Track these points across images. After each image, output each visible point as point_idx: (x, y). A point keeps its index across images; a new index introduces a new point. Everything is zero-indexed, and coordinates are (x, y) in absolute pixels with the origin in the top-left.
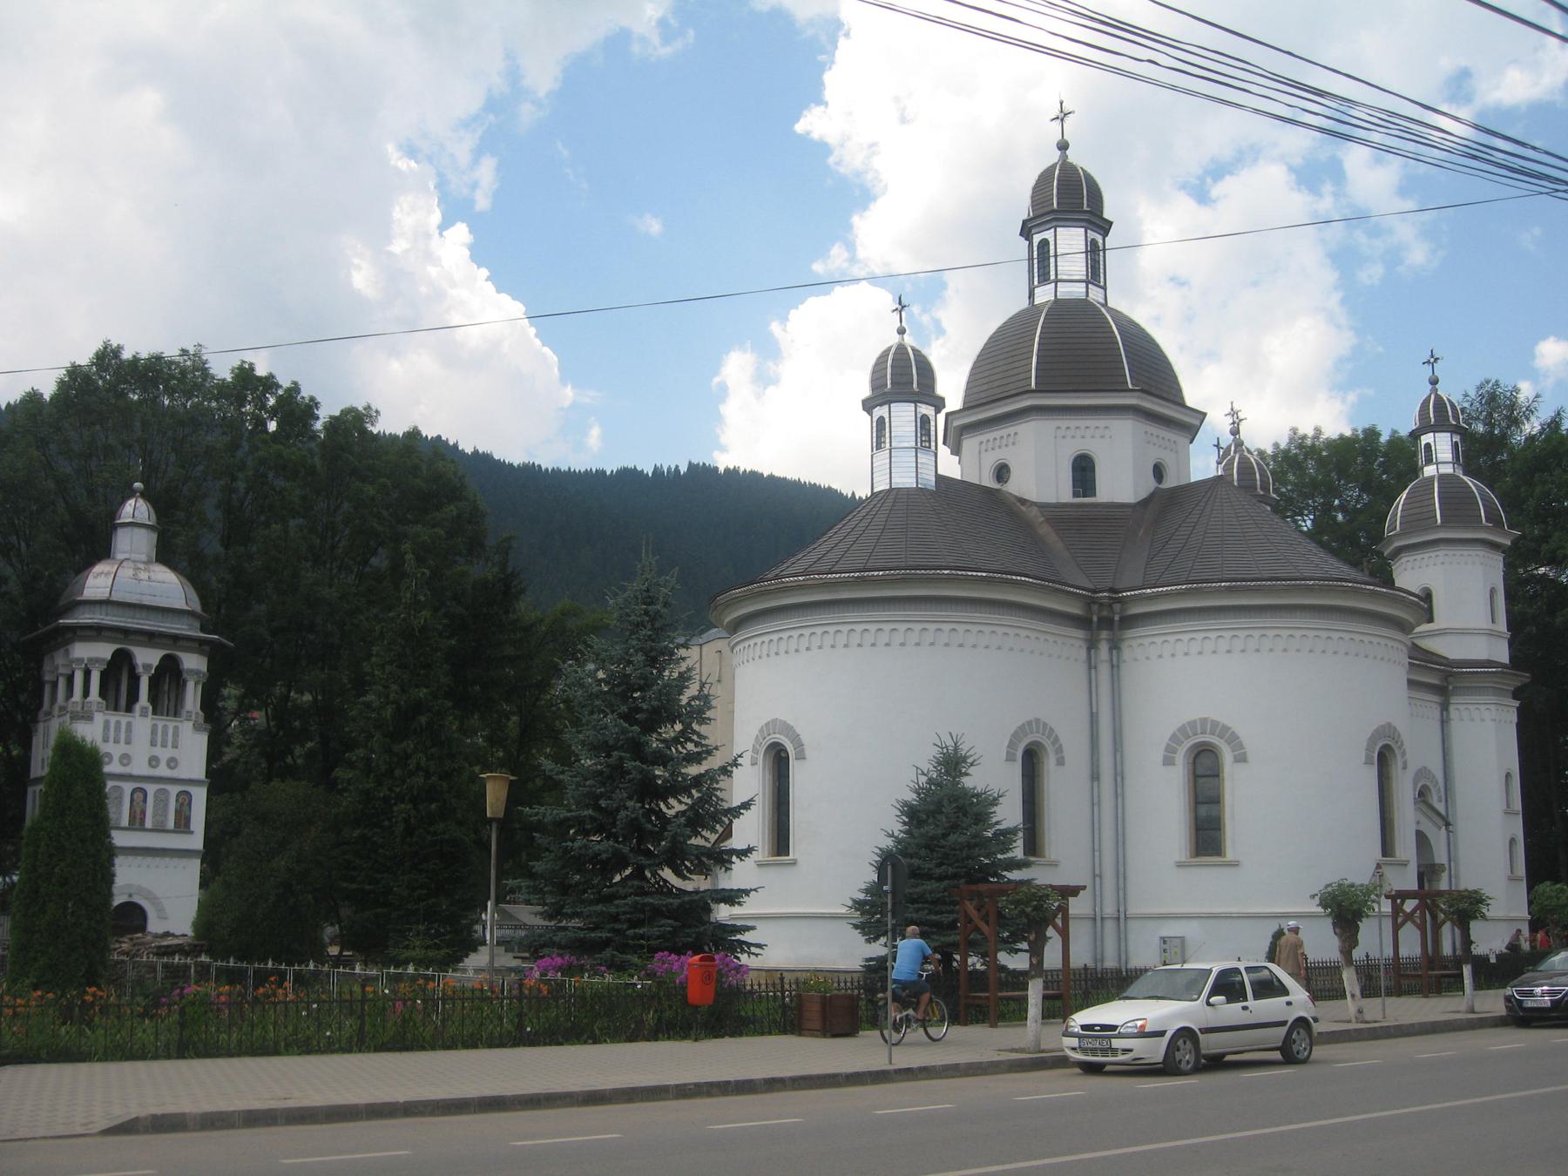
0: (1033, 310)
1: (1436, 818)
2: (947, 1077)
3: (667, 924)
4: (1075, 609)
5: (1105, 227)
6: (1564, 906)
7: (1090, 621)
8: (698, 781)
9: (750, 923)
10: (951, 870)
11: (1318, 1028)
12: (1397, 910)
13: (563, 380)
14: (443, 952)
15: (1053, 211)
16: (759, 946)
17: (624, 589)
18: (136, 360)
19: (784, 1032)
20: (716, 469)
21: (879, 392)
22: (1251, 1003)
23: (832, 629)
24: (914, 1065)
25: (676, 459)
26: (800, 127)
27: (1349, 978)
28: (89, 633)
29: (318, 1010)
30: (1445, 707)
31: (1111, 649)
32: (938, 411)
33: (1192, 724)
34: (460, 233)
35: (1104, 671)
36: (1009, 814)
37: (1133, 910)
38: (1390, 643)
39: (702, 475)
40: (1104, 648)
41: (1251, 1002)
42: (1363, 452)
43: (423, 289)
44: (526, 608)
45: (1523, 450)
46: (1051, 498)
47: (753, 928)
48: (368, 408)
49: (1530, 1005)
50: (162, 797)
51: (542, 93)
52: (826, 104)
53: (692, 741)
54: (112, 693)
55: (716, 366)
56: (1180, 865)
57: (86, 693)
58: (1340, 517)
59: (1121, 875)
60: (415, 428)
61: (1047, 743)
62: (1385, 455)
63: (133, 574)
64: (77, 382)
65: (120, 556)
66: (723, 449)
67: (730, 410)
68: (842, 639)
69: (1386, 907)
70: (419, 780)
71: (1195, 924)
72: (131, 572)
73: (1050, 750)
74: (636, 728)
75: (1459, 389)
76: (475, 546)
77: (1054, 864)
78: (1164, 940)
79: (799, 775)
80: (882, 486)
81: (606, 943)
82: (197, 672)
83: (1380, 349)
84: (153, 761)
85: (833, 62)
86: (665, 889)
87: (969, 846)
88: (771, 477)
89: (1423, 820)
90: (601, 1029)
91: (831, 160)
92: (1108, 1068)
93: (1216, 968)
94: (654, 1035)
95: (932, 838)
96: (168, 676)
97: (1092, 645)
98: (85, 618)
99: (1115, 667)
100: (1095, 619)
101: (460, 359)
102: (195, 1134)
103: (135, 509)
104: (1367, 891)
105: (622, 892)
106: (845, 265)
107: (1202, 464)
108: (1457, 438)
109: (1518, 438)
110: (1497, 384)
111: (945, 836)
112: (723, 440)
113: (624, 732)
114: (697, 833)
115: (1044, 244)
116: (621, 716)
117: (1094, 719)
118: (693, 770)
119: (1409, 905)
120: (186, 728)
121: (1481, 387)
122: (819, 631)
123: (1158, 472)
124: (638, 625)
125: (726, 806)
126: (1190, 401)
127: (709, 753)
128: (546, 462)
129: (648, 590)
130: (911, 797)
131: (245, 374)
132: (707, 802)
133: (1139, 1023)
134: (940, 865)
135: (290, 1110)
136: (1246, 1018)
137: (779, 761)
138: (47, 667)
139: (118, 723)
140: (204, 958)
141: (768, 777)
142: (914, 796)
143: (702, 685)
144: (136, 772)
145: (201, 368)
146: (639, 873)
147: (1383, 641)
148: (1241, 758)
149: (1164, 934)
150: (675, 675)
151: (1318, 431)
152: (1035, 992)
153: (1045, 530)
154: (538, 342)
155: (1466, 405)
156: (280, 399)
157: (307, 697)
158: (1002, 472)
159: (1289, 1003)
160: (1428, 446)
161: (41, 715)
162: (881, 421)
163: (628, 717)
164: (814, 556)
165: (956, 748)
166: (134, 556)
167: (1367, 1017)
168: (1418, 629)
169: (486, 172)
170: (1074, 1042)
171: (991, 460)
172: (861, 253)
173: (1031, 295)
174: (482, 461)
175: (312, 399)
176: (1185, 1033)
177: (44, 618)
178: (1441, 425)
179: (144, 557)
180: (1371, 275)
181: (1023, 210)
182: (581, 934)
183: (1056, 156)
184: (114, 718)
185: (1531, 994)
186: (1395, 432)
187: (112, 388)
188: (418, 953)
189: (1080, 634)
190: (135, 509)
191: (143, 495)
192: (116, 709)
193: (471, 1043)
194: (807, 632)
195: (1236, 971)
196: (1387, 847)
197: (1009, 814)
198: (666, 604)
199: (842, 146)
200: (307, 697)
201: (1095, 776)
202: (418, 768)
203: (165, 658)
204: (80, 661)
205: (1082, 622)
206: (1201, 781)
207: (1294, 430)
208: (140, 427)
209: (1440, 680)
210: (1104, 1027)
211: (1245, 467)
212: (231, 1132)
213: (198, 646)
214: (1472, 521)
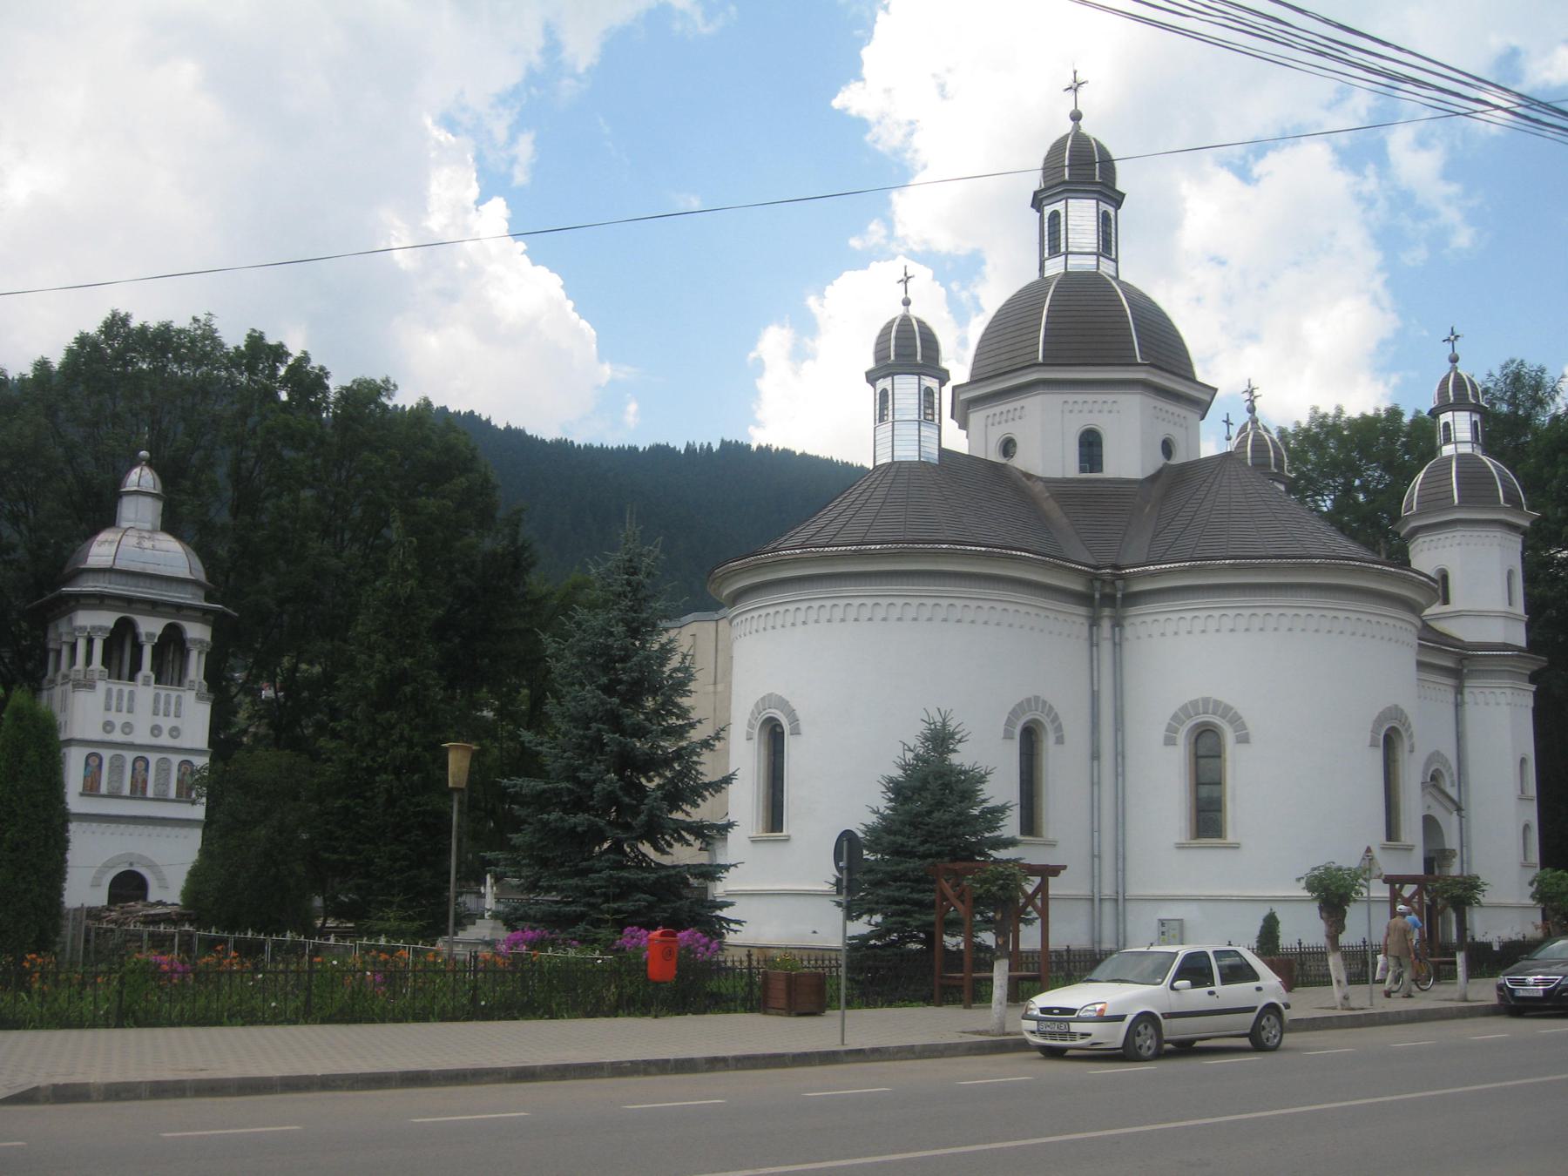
0: (1043, 281)
1: (1449, 804)
2: (901, 1059)
3: (641, 900)
4: (1077, 586)
5: (1117, 199)
6: (1564, 894)
7: (1093, 597)
8: (678, 755)
9: (729, 900)
10: (935, 848)
11: (1289, 1015)
12: (1395, 897)
13: (601, 360)
14: (417, 924)
15: (1064, 182)
16: (738, 922)
17: (606, 559)
18: (143, 329)
19: (752, 1010)
20: (749, 446)
21: (882, 363)
22: (1218, 987)
23: (828, 603)
24: (867, 1046)
25: (709, 435)
26: (836, 103)
27: (1335, 964)
28: (93, 601)
29: (264, 980)
30: (1459, 690)
31: (1113, 627)
32: (942, 383)
33: (1194, 703)
34: (497, 209)
35: (1106, 647)
36: (1001, 790)
37: (1133, 890)
38: (1399, 624)
39: (734, 453)
40: (1106, 625)
41: (1218, 987)
42: (1385, 431)
43: (461, 265)
44: (537, 582)
45: (1549, 429)
46: (1055, 472)
47: (732, 904)
48: (387, 381)
49: (1521, 993)
50: (164, 767)
51: (581, 69)
52: (863, 80)
53: (673, 714)
54: (115, 662)
55: (753, 341)
56: (1180, 847)
57: (89, 661)
58: (1361, 497)
59: (1120, 857)
60: (426, 399)
61: (1046, 721)
62: (1408, 435)
63: (138, 543)
64: (85, 352)
65: (125, 525)
66: (758, 424)
67: (766, 385)
68: (838, 613)
69: (1380, 891)
70: (403, 750)
71: (1194, 906)
72: (134, 541)
73: (1049, 727)
74: (616, 700)
75: (1482, 368)
76: (486, 518)
77: (1052, 844)
78: (1162, 923)
79: (795, 752)
80: (884, 459)
81: (581, 917)
82: (201, 642)
83: (1425, 333)
84: (156, 730)
85: (870, 38)
86: (642, 862)
87: (956, 824)
88: (804, 455)
89: (1434, 804)
90: (558, 1005)
91: (868, 138)
92: (1069, 1053)
93: (1182, 951)
94: (613, 1012)
95: (918, 815)
96: (172, 646)
97: (1094, 622)
98: (87, 586)
99: (1117, 645)
100: (1097, 596)
101: (495, 334)
102: (100, 1105)
103: (141, 478)
104: (1355, 875)
105: (598, 865)
106: (883, 241)
107: (1211, 442)
108: (1476, 417)
109: (1544, 419)
110: (1522, 363)
111: (929, 813)
112: (759, 416)
113: (603, 703)
114: (679, 808)
115: (1055, 215)
116: (598, 687)
117: (1095, 697)
118: (669, 745)
119: (1408, 890)
120: (189, 697)
121: (1505, 367)
122: (816, 604)
123: (1167, 448)
124: (619, 595)
125: (706, 780)
126: (1201, 376)
127: (692, 726)
128: (580, 439)
129: (630, 560)
130: (897, 773)
131: (256, 341)
132: (686, 776)
133: (1098, 1007)
134: (923, 843)
135: (200, 1081)
136: (1212, 1003)
137: (774, 736)
138: (51, 635)
139: (120, 692)
140: (187, 927)
141: (764, 752)
142: (901, 772)
143: (685, 657)
144: (138, 741)
145: (210, 335)
146: (617, 847)
147: (1391, 622)
148: (1244, 739)
149: (1164, 916)
150: (656, 646)
151: (1340, 411)
152: (1000, 973)
153: (1051, 507)
154: (575, 316)
155: (1490, 385)
156: (291, 369)
157: (317, 669)
158: (1008, 446)
159: (1259, 989)
160: (1447, 425)
161: (45, 682)
162: (884, 393)
163: (608, 689)
164: (813, 529)
165: (944, 724)
166: (140, 525)
167: (1353, 1005)
168: (1428, 612)
169: (525, 147)
170: (1033, 1025)
171: (996, 435)
172: (900, 231)
173: (1042, 268)
174: (515, 437)
175: (322, 369)
176: (1146, 1018)
177: (48, 587)
178: (1460, 404)
179: (148, 526)
180: (1417, 256)
181: (1035, 182)
182: (555, 908)
183: (1068, 126)
184: (116, 686)
185: (1523, 983)
186: (1418, 412)
187: (120, 355)
188: (393, 924)
189: (1082, 610)
190: (141, 478)
191: (150, 464)
192: (119, 678)
193: (422, 1016)
194: (804, 606)
195: (1205, 954)
196: (1392, 831)
197: (1001, 790)
198: (649, 575)
199: (879, 122)
200: (317, 669)
201: (1095, 756)
202: (402, 738)
203: (169, 627)
204: (83, 629)
205: (1084, 599)
206: (1202, 761)
207: (1315, 410)
208: (146, 398)
209: (1452, 662)
210: (1064, 1011)
211: (1260, 445)
212: (137, 1103)
213: (202, 615)
214: (1491, 501)
